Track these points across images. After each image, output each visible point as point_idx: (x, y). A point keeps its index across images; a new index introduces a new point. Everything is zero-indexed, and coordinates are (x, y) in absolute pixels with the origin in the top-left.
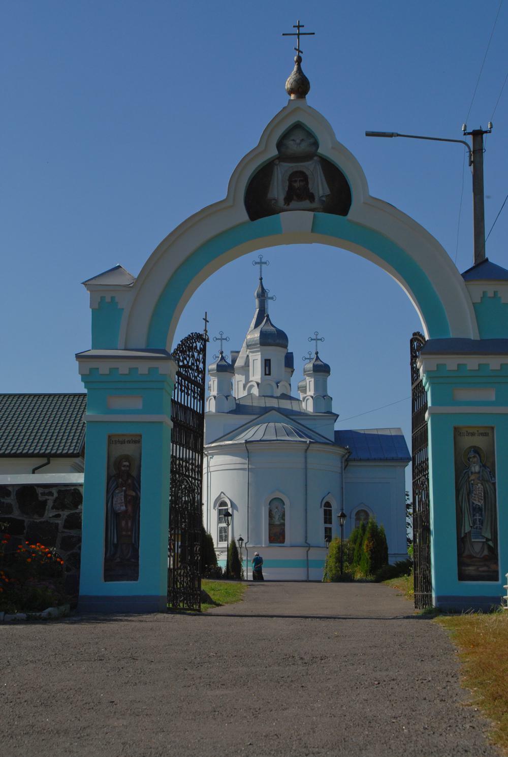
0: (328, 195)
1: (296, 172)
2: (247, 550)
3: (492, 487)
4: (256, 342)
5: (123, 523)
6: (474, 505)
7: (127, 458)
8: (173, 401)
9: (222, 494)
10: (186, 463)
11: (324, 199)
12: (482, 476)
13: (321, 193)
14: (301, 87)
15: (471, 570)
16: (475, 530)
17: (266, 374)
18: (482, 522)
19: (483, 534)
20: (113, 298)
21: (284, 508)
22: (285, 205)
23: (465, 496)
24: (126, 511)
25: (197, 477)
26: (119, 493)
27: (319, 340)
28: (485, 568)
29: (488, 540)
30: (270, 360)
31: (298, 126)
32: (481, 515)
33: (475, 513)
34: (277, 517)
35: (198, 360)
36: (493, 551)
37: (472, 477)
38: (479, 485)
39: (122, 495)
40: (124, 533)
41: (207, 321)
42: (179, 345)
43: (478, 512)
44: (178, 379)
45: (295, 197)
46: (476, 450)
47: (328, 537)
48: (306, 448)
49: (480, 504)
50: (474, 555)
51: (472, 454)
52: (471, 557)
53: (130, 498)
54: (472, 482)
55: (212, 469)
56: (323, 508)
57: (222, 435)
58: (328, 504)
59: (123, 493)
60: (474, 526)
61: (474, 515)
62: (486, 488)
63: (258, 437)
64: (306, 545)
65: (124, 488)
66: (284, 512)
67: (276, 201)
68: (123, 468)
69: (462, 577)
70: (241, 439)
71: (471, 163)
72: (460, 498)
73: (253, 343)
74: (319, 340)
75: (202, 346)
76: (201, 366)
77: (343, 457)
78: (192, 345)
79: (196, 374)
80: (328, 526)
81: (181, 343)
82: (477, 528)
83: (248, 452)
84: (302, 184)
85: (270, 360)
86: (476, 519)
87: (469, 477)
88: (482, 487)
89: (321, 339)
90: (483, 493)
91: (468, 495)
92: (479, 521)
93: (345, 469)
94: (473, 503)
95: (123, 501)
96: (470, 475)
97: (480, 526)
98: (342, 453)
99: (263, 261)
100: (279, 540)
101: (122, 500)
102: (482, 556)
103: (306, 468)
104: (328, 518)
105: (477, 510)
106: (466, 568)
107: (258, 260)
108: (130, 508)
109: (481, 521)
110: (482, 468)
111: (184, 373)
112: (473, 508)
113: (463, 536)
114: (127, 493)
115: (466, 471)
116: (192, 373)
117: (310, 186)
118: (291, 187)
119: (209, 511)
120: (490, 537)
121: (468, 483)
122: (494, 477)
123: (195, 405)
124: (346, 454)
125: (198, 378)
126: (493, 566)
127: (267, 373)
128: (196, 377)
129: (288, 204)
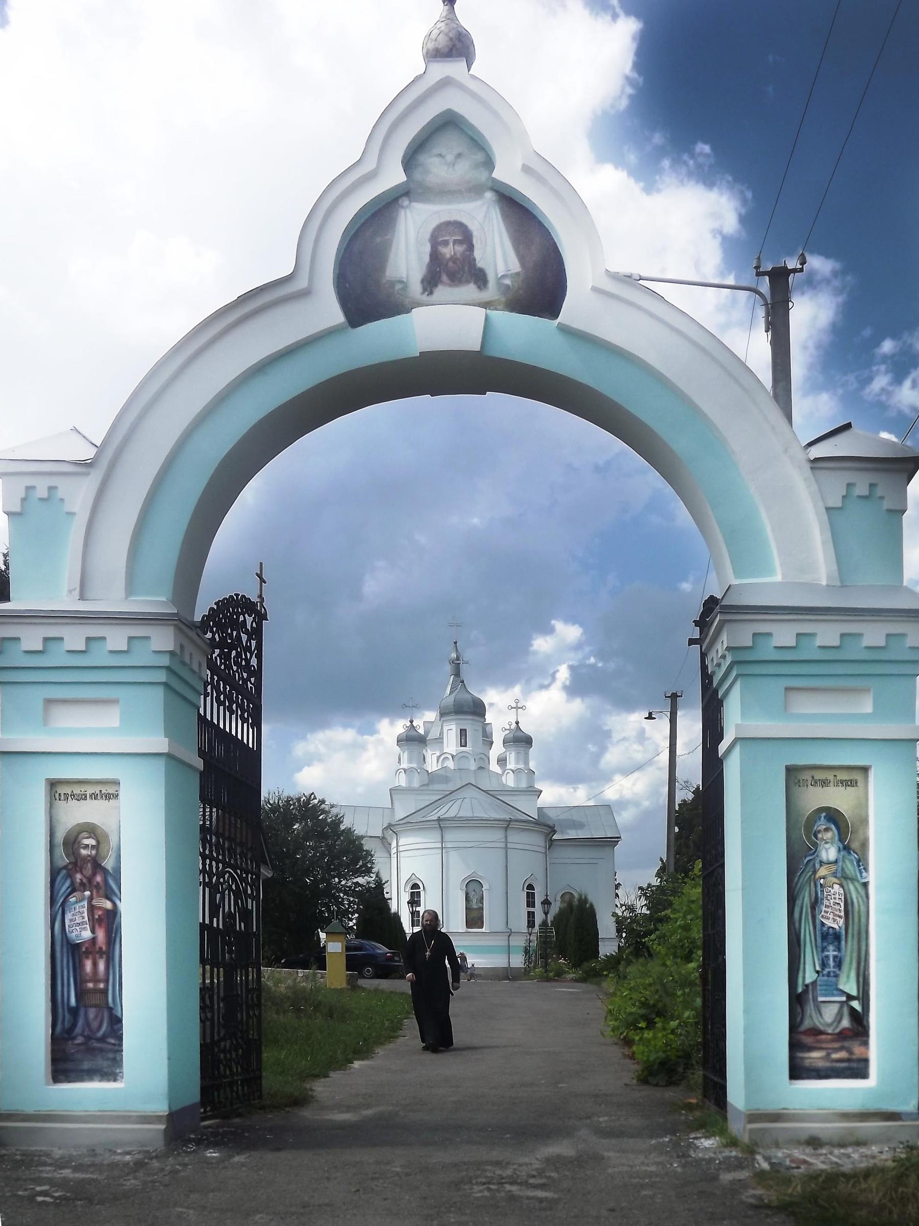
0: (517, 274)
1: (448, 224)
3: (863, 892)
5: (88, 965)
6: (825, 929)
7: (91, 830)
8: (202, 719)
10: (218, 838)
11: (507, 282)
12: (843, 869)
13: (501, 271)
14: (455, 46)
15: (815, 1057)
16: (825, 978)
18: (839, 963)
19: (841, 987)
20: (52, 489)
22: (423, 293)
23: (806, 912)
24: (94, 940)
25: (214, 863)
26: (76, 902)
28: (842, 1054)
29: (850, 997)
31: (448, 123)
32: (839, 949)
33: (825, 944)
35: (248, 649)
36: (860, 1021)
37: (822, 872)
38: (836, 887)
39: (83, 907)
40: (90, 985)
41: (263, 581)
42: (212, 609)
43: (832, 943)
44: (212, 679)
45: (445, 278)
46: (833, 816)
49: (836, 926)
50: (822, 1028)
51: (822, 824)
52: (816, 1032)
53: (100, 913)
54: (822, 881)
55: (401, 849)
58: (530, 887)
59: (85, 903)
60: (823, 969)
61: (824, 949)
62: (850, 893)
63: (451, 814)
65: (87, 893)
67: (405, 285)
68: (84, 852)
69: (797, 1071)
72: (796, 915)
75: (254, 625)
76: (254, 662)
78: (238, 618)
79: (245, 675)
80: (531, 909)
81: (215, 607)
82: (828, 975)
84: (460, 249)
86: (827, 957)
87: (815, 872)
88: (842, 892)
90: (842, 905)
91: (813, 907)
92: (834, 961)
94: (823, 924)
95: (86, 919)
96: (817, 866)
97: (836, 970)
101: (83, 918)
102: (837, 1031)
103: (506, 848)
104: (531, 903)
105: (832, 937)
106: (807, 1055)
108: (101, 935)
109: (837, 960)
110: (842, 853)
111: (223, 667)
112: (822, 934)
113: (800, 990)
114: (94, 902)
115: (808, 859)
116: (237, 671)
117: (477, 254)
118: (435, 256)
120: (854, 993)
121: (812, 884)
122: (866, 869)
123: (249, 739)
125: (250, 685)
126: (858, 1050)
128: (245, 681)
129: (431, 293)
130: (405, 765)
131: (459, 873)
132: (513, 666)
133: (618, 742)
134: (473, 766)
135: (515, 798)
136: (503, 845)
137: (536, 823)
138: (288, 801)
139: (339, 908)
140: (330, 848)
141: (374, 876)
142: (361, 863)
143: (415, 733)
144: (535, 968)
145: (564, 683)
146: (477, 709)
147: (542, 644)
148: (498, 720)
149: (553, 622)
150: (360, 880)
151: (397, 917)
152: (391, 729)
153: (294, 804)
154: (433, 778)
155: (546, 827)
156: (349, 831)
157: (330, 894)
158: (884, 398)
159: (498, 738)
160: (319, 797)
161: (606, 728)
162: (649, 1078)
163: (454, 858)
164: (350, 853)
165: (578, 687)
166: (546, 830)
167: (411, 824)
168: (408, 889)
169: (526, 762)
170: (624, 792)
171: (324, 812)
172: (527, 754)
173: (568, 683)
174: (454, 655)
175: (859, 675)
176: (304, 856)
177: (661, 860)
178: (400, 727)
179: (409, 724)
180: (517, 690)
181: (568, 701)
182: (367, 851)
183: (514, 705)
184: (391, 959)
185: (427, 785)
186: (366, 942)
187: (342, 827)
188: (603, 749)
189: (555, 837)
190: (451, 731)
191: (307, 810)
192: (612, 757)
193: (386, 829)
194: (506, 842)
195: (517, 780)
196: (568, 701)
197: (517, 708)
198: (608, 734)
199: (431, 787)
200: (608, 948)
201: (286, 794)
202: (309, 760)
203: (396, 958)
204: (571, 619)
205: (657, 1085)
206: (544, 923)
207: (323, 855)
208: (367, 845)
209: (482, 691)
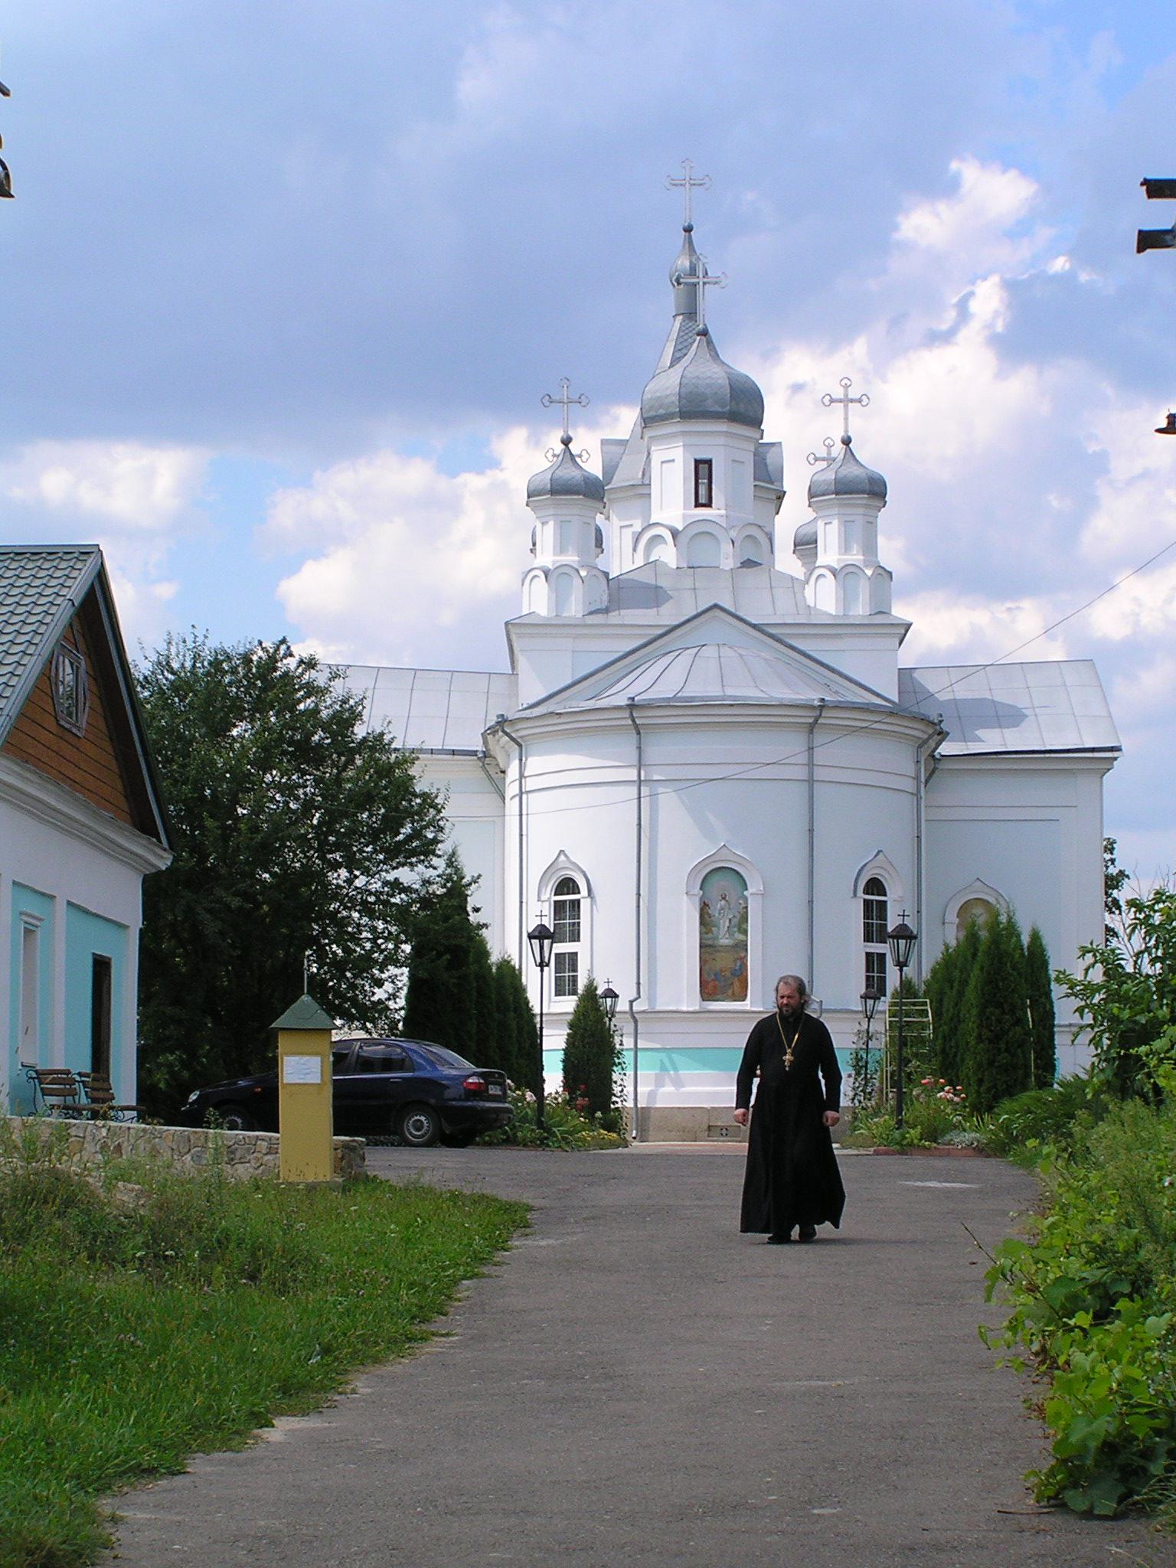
2: (636, 1022)
9: (562, 858)
17: (697, 505)
21: (746, 899)
27: (852, 401)
30: (709, 462)
55: (530, 784)
57: (569, 682)
58: (875, 886)
63: (665, 689)
71: (176, 1471)
73: (661, 411)
74: (852, 401)
77: (920, 747)
85: (709, 462)
93: (927, 782)
100: (730, 992)
103: (811, 781)
124: (930, 737)
127: (702, 500)
130: (547, 557)
131: (684, 847)
132: (848, 284)
133: (1131, 482)
134: (727, 559)
135: (842, 644)
136: (801, 773)
137: (892, 714)
138: (216, 664)
139: (347, 951)
140: (330, 788)
141: (440, 863)
142: (407, 830)
143: (576, 474)
144: (876, 1113)
145: (990, 326)
146: (743, 407)
147: (924, 225)
148: (797, 431)
149: (954, 166)
150: (406, 876)
151: (509, 978)
152: (524, 455)
153: (234, 671)
154: (620, 593)
155: (920, 727)
156: (376, 744)
159: (796, 481)
160: (301, 650)
161: (1093, 448)
162: (1069, 1495)
163: (670, 806)
164: (384, 802)
165: (1035, 329)
166: (919, 731)
167: (560, 720)
168: (549, 895)
169: (870, 548)
170: (1145, 620)
171: (312, 690)
172: (871, 524)
173: (999, 327)
174: (684, 263)
175: (638, 907)
176: (258, 810)
178: (524, 455)
179: (559, 448)
180: (860, 348)
181: (1000, 375)
182: (425, 796)
183: (839, 393)
184: (478, 1093)
185: (606, 611)
186: (413, 1046)
187: (360, 731)
188: (1088, 504)
190: (670, 467)
191: (269, 685)
192: (1113, 522)
193: (492, 731)
194: (811, 764)
195: (846, 597)
196: (1000, 375)
198: (1099, 465)
199: (614, 618)
200: (1075, 1057)
201: (213, 643)
202: (319, 542)
203: (494, 1090)
204: (1005, 158)
205: (1088, 1515)
206: (907, 989)
207: (308, 806)
208: (425, 778)
209: (770, 355)
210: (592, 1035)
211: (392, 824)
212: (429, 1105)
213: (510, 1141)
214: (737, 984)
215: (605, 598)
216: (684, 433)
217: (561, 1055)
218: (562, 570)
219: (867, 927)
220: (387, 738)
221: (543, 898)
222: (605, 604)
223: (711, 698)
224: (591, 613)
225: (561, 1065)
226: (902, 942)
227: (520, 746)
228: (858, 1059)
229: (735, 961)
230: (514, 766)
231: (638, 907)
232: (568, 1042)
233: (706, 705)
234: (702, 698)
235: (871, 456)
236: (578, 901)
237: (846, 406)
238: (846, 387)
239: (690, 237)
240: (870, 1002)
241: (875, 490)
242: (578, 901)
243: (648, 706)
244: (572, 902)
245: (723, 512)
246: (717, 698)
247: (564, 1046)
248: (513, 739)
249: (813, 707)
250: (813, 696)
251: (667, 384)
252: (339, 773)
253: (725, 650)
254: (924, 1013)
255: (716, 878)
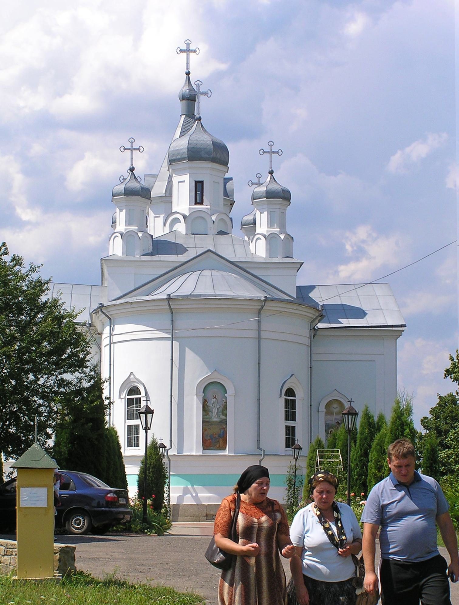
4: (183, 156)
17: (196, 203)
21: (226, 398)
27: (274, 152)
30: (202, 182)
34: (215, 411)
47: (290, 442)
48: (260, 307)
55: (115, 339)
56: (284, 397)
57: (133, 288)
58: (290, 392)
64: (258, 452)
66: (226, 402)
69: (138, 445)
70: (161, 294)
73: (179, 157)
74: (274, 152)
80: (291, 423)
83: (172, 313)
85: (202, 182)
89: (278, 153)
98: (312, 316)
99: (191, 48)
100: (218, 446)
103: (259, 338)
104: (290, 415)
107: (184, 47)
119: (112, 366)
127: (198, 201)
131: (197, 372)
136: (254, 334)
150: (67, 377)
154: (159, 247)
157: (21, 395)
158: (374, 235)
159: (242, 195)
166: (312, 314)
168: (124, 395)
172: (283, 213)
175: (171, 401)
177: (452, 359)
185: (151, 254)
187: (43, 298)
189: (320, 325)
193: (96, 312)
194: (259, 330)
197: (271, 152)
199: (156, 258)
210: (154, 467)
211: (58, 350)
212: (85, 510)
213: (128, 530)
214: (221, 441)
215: (151, 247)
216: (190, 168)
217: (137, 478)
218: (130, 233)
219: (293, 434)
220: (60, 302)
221: (122, 397)
222: (151, 250)
223: (209, 295)
224: (143, 255)
225: (137, 483)
226: (350, 417)
227: (110, 319)
228: (290, 481)
229: (221, 429)
230: (107, 330)
231: (171, 401)
232: (141, 471)
233: (206, 299)
234: (205, 295)
235: (283, 181)
236: (140, 398)
237: (271, 156)
238: (271, 146)
239: (189, 77)
240: (297, 451)
241: (285, 196)
242: (140, 398)
243: (177, 299)
244: (137, 399)
245: (209, 207)
246: (212, 295)
247: (138, 473)
248: (106, 316)
249: (260, 301)
250: (261, 295)
251: (182, 144)
252: (31, 320)
253: (213, 272)
254: (337, 457)
255: (211, 387)
